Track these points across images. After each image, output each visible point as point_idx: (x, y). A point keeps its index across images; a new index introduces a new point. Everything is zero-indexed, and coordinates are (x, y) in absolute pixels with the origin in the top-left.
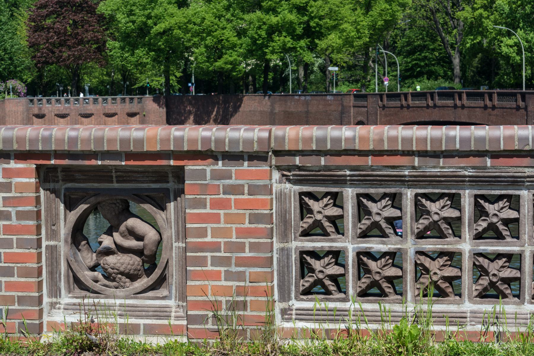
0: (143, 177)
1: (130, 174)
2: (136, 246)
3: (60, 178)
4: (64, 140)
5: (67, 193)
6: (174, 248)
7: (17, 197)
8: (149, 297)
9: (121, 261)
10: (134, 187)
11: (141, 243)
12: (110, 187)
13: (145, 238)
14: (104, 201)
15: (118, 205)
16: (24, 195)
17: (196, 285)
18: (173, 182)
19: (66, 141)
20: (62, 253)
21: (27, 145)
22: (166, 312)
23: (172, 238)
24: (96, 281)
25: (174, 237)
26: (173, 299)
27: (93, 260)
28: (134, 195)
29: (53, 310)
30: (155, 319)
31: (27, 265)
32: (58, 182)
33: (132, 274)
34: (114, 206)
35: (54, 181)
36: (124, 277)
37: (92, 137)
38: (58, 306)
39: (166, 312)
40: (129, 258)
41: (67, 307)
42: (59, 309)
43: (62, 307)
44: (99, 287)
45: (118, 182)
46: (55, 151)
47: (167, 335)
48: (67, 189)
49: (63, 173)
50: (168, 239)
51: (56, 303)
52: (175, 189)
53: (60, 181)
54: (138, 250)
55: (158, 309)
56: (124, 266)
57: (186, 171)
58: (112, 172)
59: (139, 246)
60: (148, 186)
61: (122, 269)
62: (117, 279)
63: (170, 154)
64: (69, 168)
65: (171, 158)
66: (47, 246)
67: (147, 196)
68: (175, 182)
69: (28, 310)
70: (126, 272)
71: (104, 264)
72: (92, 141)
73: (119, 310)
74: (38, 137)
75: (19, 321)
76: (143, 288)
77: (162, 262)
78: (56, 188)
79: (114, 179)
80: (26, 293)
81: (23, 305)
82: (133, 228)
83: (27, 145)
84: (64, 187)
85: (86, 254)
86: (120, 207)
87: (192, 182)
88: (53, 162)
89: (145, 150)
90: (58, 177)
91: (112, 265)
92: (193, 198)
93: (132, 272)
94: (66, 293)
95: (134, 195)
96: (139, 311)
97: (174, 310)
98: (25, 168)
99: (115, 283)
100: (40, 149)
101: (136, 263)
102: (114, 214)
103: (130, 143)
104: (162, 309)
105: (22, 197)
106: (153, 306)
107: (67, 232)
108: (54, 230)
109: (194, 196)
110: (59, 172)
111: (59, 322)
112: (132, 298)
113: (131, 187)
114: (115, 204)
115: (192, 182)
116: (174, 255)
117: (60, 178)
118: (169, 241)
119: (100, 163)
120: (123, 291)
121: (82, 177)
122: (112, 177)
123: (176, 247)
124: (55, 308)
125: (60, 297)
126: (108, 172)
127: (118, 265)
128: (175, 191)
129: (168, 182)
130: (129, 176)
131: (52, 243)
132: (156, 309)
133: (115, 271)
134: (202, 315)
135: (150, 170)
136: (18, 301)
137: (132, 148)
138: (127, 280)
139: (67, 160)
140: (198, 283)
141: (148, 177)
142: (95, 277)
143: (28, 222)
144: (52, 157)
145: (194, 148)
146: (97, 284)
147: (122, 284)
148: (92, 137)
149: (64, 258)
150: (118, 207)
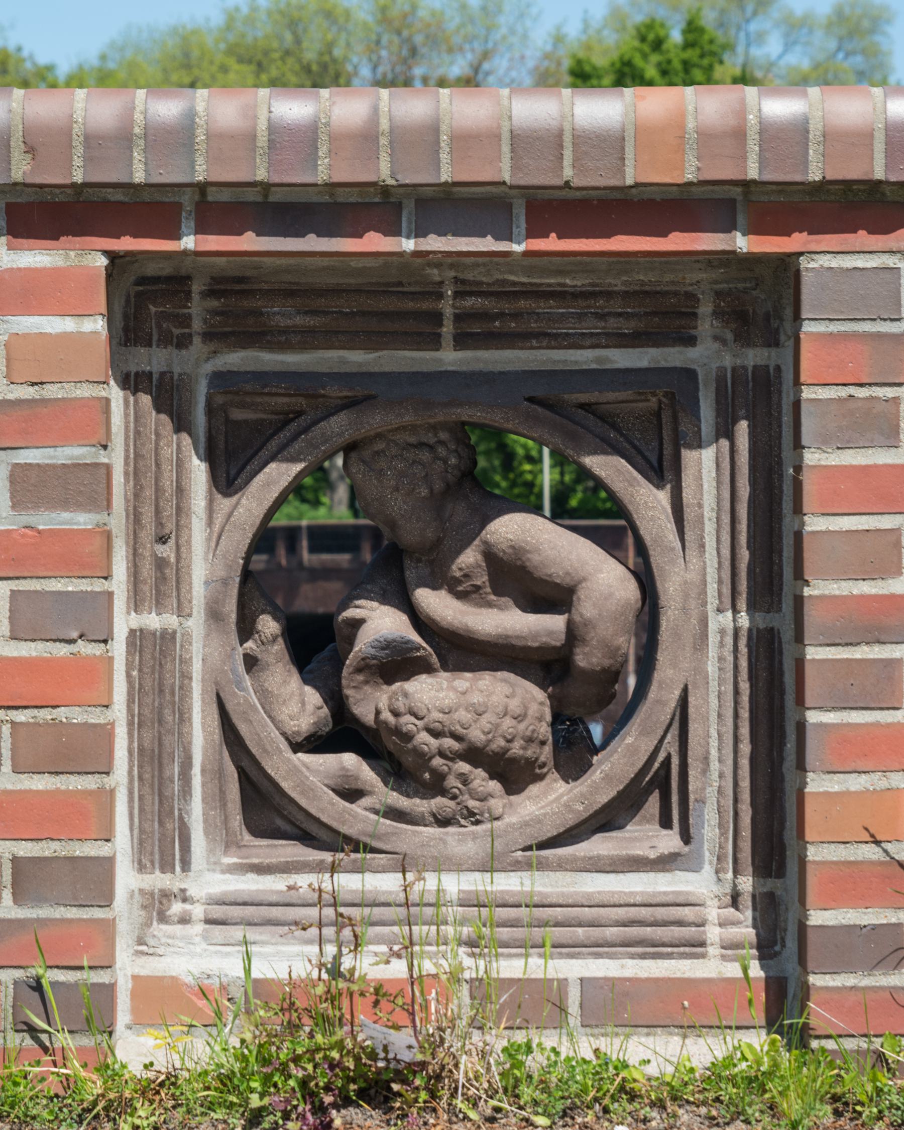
0: (580, 317)
1: (522, 303)
2: (536, 636)
3: (197, 325)
4: (254, 137)
5: (220, 400)
6: (713, 639)
7: (19, 402)
8: (599, 858)
9: (476, 698)
10: (534, 367)
11: (554, 623)
12: (425, 369)
13: (581, 593)
14: (379, 436)
15: (441, 451)
16: (52, 392)
17: (848, 793)
18: (716, 338)
19: (262, 140)
20: (197, 668)
21: (77, 162)
22: (680, 923)
23: (704, 592)
24: (351, 794)
25: (712, 589)
26: (708, 870)
27: (310, 708)
28: (531, 400)
29: (158, 929)
30: (632, 956)
31: (62, 714)
32: (183, 343)
33: (514, 760)
34: (425, 456)
35: (166, 340)
36: (480, 773)
37: (384, 124)
38: (177, 908)
39: (680, 923)
40: (507, 690)
41: (218, 912)
42: (184, 920)
43: (198, 911)
44: (365, 820)
45: (462, 341)
46: (202, 188)
47: (687, 1029)
48: (219, 379)
49: (214, 303)
50: (686, 596)
51: (166, 896)
52: (722, 370)
53: (197, 340)
54: (543, 649)
55: (644, 913)
56: (485, 722)
57: (808, 283)
58: (440, 296)
59: (550, 633)
60: (598, 360)
61: (476, 735)
62: (452, 782)
63: (732, 202)
64: (241, 280)
65: (741, 219)
66: (132, 632)
67: (582, 406)
68: (724, 342)
69: (63, 921)
70: (494, 746)
71: (396, 714)
72: (383, 141)
73: (463, 922)
74: (132, 121)
75: (18, 974)
76: (571, 820)
77: (658, 702)
78: (177, 370)
79: (447, 329)
80: (55, 845)
81: (40, 900)
82: (518, 551)
83: (77, 162)
84: (209, 367)
85: (278, 678)
86: (453, 461)
87: (834, 328)
88: (189, 242)
89: (629, 181)
90: (186, 321)
91: (436, 715)
92: (840, 400)
93: (516, 749)
94: (211, 851)
95: (531, 400)
96: (557, 924)
97: (713, 913)
98: (54, 272)
99: (438, 802)
100: (139, 177)
101: (533, 709)
102: (424, 492)
103: (561, 146)
104: (661, 913)
105: (44, 401)
106: (615, 900)
107: (221, 573)
108: (160, 563)
109: (843, 392)
110: (196, 297)
111: (189, 980)
112: (517, 866)
113: (518, 367)
114: (431, 448)
115: (834, 328)
116: (712, 668)
117: (197, 325)
118: (693, 604)
119: (409, 245)
120: (474, 836)
121: (299, 320)
122: (437, 318)
123: (722, 632)
124: (163, 918)
125: (186, 865)
126: (425, 295)
127: (463, 715)
128: (720, 380)
129: (691, 341)
130: (516, 316)
131: (153, 621)
132: (633, 912)
133: (449, 743)
134: (874, 927)
135: (617, 283)
136: (15, 884)
137: (568, 173)
138: (494, 786)
139: (250, 235)
140: (856, 783)
141: (602, 317)
142: (346, 775)
143: (66, 515)
144: (188, 224)
145: (853, 172)
146: (357, 808)
147: (472, 804)
148: (384, 124)
149: (204, 692)
150: (445, 461)
